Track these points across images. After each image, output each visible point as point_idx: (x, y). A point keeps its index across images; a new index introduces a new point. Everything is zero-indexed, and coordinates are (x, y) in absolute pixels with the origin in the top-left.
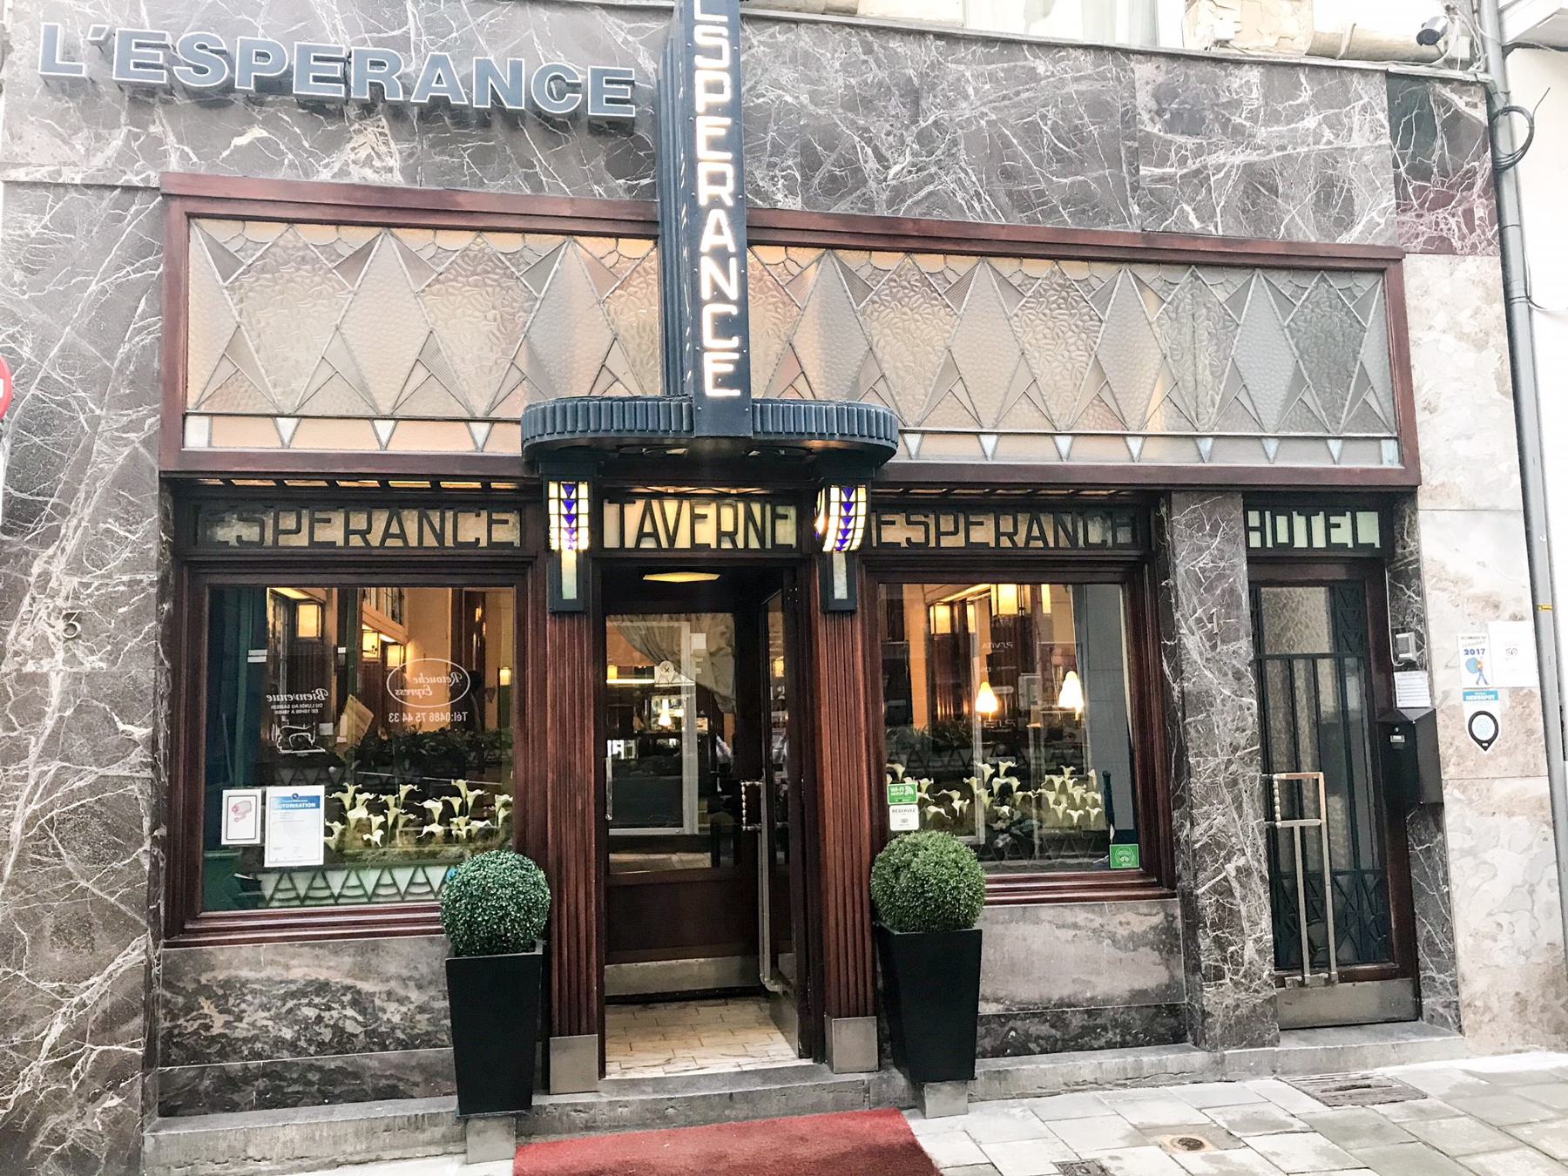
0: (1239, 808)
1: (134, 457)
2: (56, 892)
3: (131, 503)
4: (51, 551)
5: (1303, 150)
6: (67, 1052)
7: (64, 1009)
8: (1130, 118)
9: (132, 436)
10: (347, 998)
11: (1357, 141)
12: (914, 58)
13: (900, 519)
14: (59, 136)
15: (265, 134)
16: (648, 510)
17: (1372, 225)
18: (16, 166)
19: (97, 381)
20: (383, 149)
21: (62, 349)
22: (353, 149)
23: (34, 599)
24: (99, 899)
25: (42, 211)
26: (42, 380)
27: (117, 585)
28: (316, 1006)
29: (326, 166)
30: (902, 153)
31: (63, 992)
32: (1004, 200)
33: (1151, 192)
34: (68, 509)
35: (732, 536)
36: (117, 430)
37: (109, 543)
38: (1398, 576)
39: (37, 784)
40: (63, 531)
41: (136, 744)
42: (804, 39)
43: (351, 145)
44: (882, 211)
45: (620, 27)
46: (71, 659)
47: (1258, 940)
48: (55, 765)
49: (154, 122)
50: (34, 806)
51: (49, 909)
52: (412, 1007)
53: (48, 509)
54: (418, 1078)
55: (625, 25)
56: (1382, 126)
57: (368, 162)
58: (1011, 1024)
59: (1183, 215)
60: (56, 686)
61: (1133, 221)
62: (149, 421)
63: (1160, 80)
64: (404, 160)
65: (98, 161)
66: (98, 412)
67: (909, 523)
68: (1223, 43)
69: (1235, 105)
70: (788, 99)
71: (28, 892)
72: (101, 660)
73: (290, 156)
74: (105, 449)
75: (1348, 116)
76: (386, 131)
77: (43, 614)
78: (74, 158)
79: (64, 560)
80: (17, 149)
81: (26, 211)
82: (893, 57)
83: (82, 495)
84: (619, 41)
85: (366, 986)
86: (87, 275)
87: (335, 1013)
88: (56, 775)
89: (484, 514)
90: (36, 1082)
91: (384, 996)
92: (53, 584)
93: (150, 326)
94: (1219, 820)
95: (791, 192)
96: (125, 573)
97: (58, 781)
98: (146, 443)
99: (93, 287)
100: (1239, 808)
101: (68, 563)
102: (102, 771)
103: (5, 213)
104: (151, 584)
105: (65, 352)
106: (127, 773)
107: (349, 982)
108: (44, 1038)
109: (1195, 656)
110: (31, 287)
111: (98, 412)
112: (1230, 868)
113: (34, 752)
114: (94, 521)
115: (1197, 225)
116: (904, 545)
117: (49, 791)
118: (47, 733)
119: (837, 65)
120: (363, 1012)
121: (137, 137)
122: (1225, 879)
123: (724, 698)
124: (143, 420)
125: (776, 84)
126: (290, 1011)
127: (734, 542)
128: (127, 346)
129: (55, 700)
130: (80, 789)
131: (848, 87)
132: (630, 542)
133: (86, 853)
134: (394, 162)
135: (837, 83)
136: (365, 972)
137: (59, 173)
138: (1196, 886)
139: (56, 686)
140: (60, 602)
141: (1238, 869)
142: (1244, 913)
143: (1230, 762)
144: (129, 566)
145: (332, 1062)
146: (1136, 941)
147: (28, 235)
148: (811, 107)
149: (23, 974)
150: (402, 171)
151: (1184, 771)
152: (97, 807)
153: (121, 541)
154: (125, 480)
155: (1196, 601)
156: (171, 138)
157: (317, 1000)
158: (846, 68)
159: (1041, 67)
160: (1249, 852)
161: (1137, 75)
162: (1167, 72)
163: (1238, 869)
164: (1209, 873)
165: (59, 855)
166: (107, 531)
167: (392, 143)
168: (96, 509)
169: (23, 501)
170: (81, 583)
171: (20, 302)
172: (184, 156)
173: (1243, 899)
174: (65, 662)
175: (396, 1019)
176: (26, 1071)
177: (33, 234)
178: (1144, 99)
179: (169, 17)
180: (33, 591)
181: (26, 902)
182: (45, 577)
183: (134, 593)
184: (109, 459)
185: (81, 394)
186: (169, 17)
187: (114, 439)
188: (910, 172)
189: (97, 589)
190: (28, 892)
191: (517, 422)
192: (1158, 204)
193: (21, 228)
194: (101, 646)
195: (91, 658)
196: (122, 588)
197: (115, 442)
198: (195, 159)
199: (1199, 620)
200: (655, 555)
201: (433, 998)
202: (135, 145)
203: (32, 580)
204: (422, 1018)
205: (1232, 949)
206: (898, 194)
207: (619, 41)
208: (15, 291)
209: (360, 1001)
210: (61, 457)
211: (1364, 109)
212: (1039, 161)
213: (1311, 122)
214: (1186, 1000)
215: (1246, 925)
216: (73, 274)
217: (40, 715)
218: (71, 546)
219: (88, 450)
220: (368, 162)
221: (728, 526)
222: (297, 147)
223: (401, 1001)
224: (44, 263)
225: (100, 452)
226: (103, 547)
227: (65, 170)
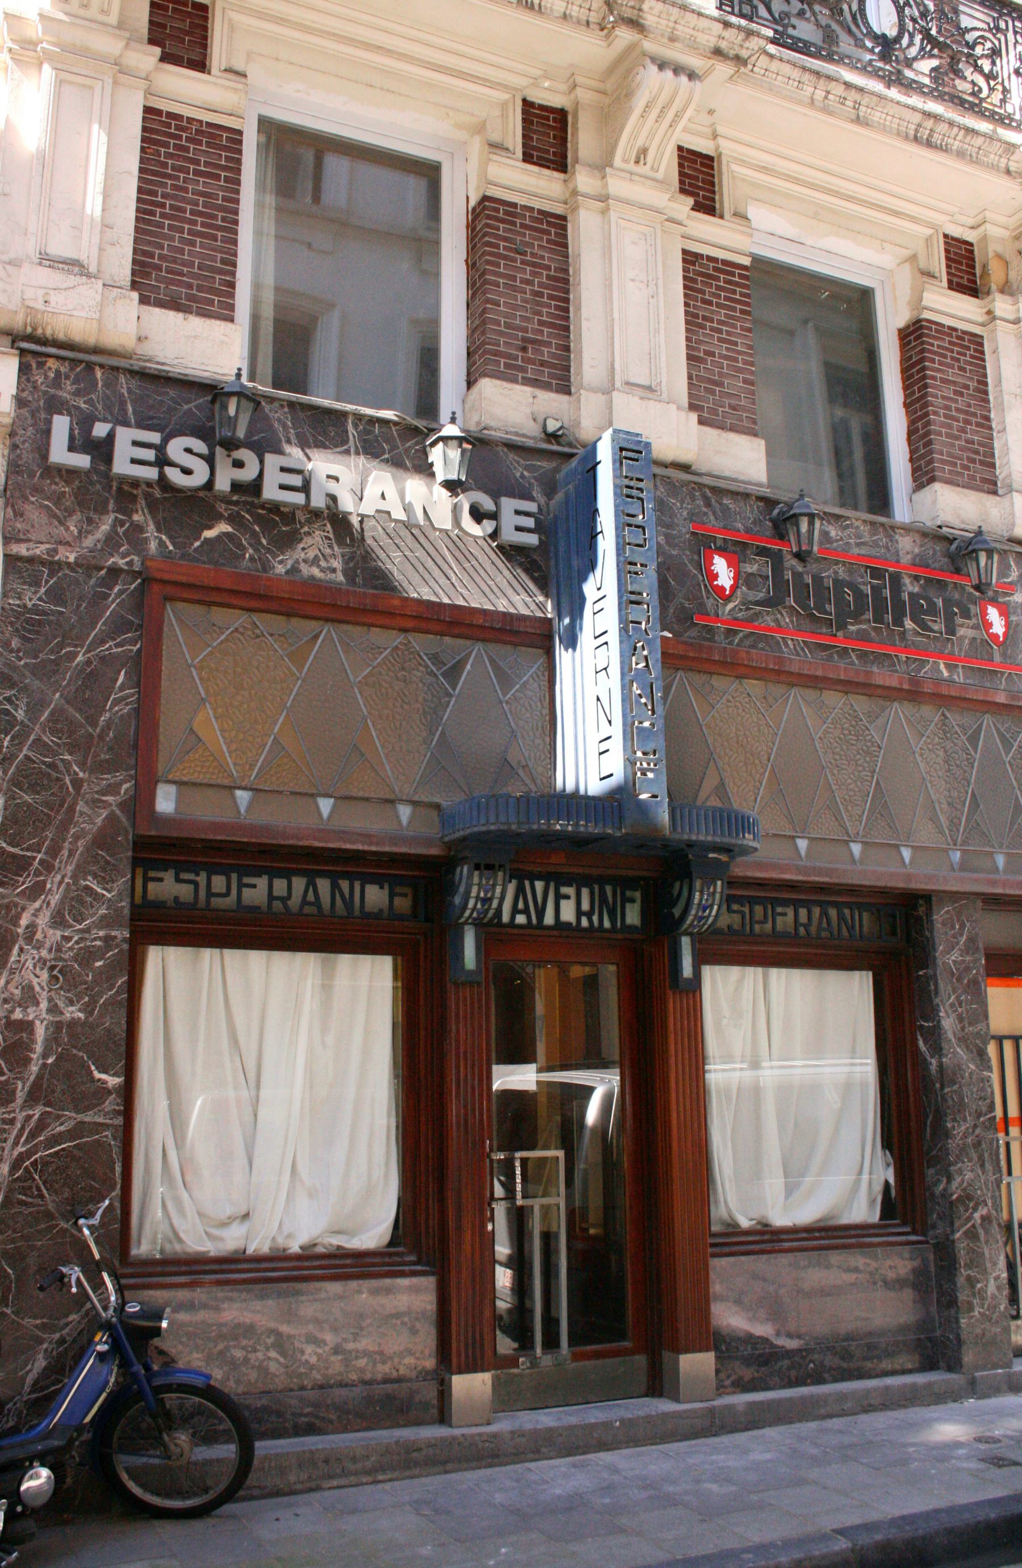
0: (982, 1165)
1: (111, 818)
2: (38, 1231)
3: (107, 862)
4: (37, 904)
6: (48, 1387)
7: (45, 1346)
9: (110, 799)
10: (270, 1341)
14: (55, 516)
15: (230, 529)
16: (520, 891)
18: (19, 541)
19: (80, 746)
20: (328, 551)
21: (52, 714)
22: (303, 549)
23: (21, 950)
25: (37, 584)
26: (34, 741)
27: (95, 939)
28: (243, 1348)
29: (281, 562)
31: (44, 1327)
34: (53, 866)
36: (97, 792)
37: (89, 899)
39: (23, 1128)
40: (48, 886)
41: (109, 1092)
43: (301, 546)
45: (518, 463)
46: (53, 1009)
47: (997, 1278)
48: (37, 1112)
49: (137, 511)
50: (21, 1149)
51: (32, 1248)
52: (327, 1348)
53: (36, 863)
54: (333, 1417)
55: (522, 462)
57: (315, 561)
58: (810, 1357)
60: (40, 1032)
62: (125, 786)
63: (917, 550)
64: (346, 562)
65: (89, 542)
66: (81, 775)
71: (14, 1231)
72: (80, 1010)
73: (251, 551)
74: (86, 809)
76: (331, 536)
77: (30, 964)
78: (69, 539)
79: (48, 914)
80: (19, 526)
81: (24, 583)
82: (726, 510)
83: (65, 853)
84: (518, 475)
86: (76, 646)
87: (260, 1355)
88: (40, 1120)
90: (19, 1417)
91: (303, 1339)
92: (39, 936)
93: (128, 697)
94: (969, 1176)
96: (101, 928)
97: (42, 1125)
98: (122, 805)
99: (80, 658)
100: (982, 1165)
101: (53, 917)
102: (80, 1117)
103: (4, 584)
104: (124, 940)
105: (57, 715)
106: (101, 1120)
107: (272, 1325)
108: (28, 1373)
109: (950, 1036)
110: (27, 654)
111: (81, 775)
112: (977, 1215)
113: (20, 1095)
114: (75, 877)
115: (946, 674)
117: (33, 1135)
118: (32, 1078)
119: (685, 513)
120: (283, 1353)
121: (122, 524)
122: (974, 1226)
124: (120, 784)
126: (221, 1353)
127: (590, 921)
128: (108, 715)
129: (39, 1047)
130: (60, 1133)
133: (66, 1195)
134: (337, 564)
136: (290, 1316)
137: (55, 551)
138: (953, 1232)
139: (40, 1032)
140: (44, 953)
141: (983, 1218)
142: (987, 1255)
143: (975, 1126)
144: (105, 922)
146: (899, 1284)
147: (25, 606)
149: (9, 1311)
150: (345, 572)
151: (941, 1133)
152: (75, 1152)
153: (97, 897)
154: (103, 840)
155: (950, 988)
156: (152, 527)
157: (244, 1342)
158: (692, 516)
160: (990, 1203)
161: (900, 546)
162: (921, 546)
163: (983, 1218)
164: (962, 1221)
165: (41, 1196)
166: (87, 887)
167: (336, 548)
168: (78, 866)
169: (14, 856)
170: (63, 937)
171: (15, 668)
172: (161, 544)
173: (987, 1242)
174: (49, 1011)
175: (313, 1360)
176: (10, 1405)
177: (29, 604)
179: (152, 418)
180: (21, 942)
181: (13, 1241)
182: (32, 928)
183: (108, 947)
184: (90, 819)
185: (68, 757)
186: (152, 418)
187: (95, 801)
189: (77, 943)
190: (14, 1231)
193: (20, 598)
194: (80, 998)
195: (71, 1009)
196: (98, 943)
197: (96, 803)
198: (171, 548)
199: (952, 1005)
201: (345, 1340)
202: (121, 531)
203: (20, 931)
205: (979, 1286)
207: (518, 475)
208: (12, 657)
209: (281, 1342)
210: (49, 816)
214: (938, 1333)
215: (988, 1265)
216: (61, 646)
217: (28, 1061)
218: (55, 899)
219: (72, 810)
220: (315, 561)
221: (585, 906)
222: (256, 545)
224: (38, 633)
225: (82, 813)
226: (82, 902)
227: (61, 549)
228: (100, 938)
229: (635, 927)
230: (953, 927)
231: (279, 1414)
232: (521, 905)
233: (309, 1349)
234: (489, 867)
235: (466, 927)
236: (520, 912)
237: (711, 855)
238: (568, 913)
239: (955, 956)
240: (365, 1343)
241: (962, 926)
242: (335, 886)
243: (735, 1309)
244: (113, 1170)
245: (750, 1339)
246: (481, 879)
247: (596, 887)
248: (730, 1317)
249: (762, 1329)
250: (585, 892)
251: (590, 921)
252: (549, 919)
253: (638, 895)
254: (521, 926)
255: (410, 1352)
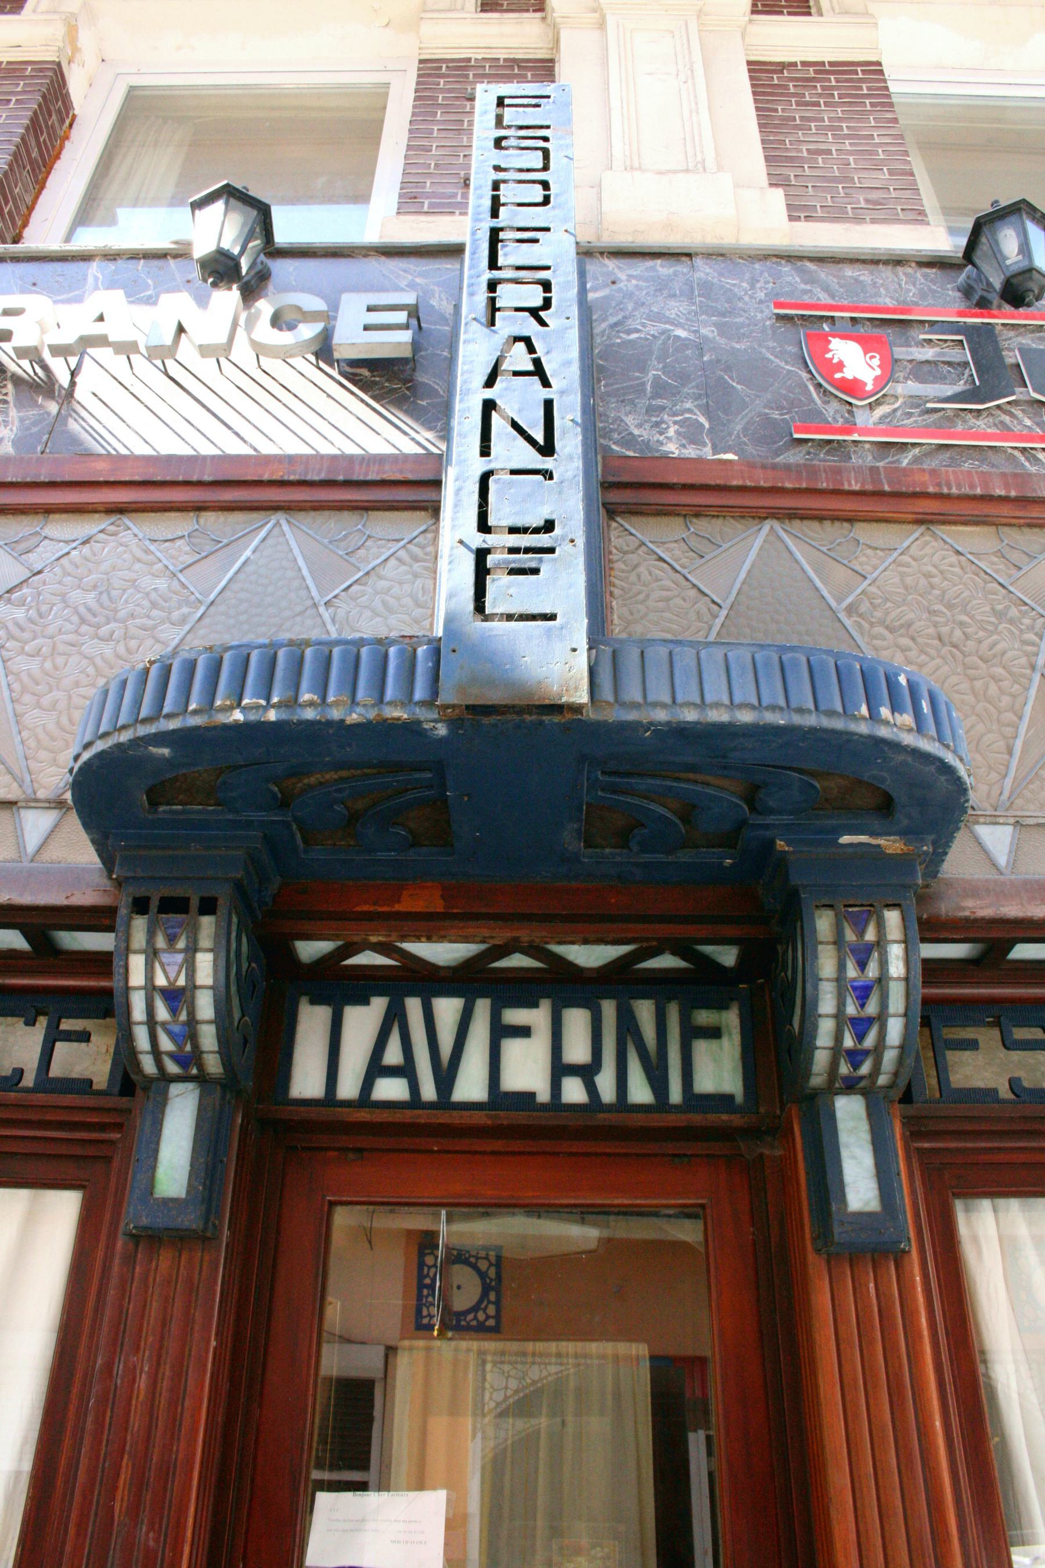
13: (988, 1037)
16: (395, 1017)
35: (587, 1073)
38: (848, 741)
67: (1009, 1044)
70: (682, 333)
89: (43, 1022)
116: (1005, 1093)
123: (61, 386)
125: (659, 318)
127: (591, 1089)
132: (348, 1088)
148: (723, 341)
188: (910, 415)
191: (129, 358)
200: (408, 1116)
221: (577, 1051)
229: (725, 1100)
232: (393, 1055)
234: (174, 905)
235: (175, 1089)
236: (393, 1072)
237: (845, 839)
238: (526, 1069)
246: (151, 935)
247: (609, 1009)
251: (591, 1089)
252: (471, 1086)
253: (731, 1019)
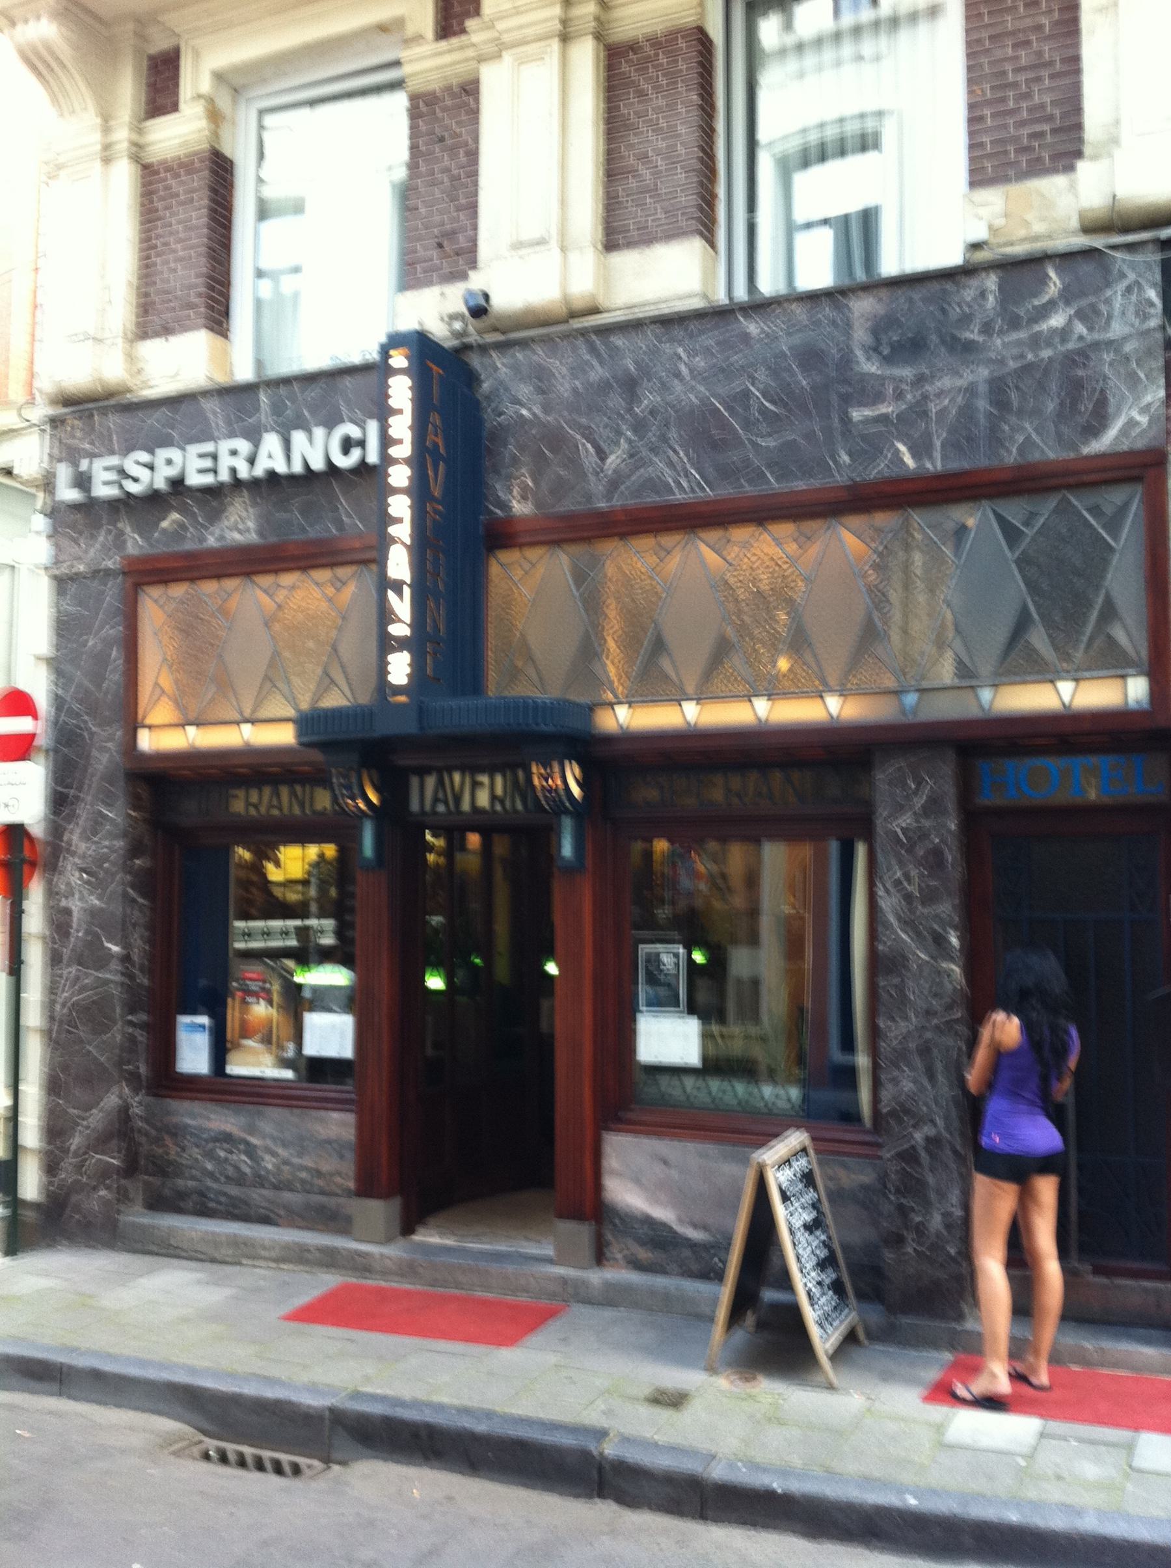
5: (1046, 353)
8: (847, 360)
9: (109, 745)
11: (1117, 329)
12: (630, 353)
16: (440, 783)
17: (1131, 423)
24: (96, 1058)
30: (617, 444)
32: (710, 471)
33: (864, 438)
42: (539, 355)
44: (602, 505)
54: (282, 1212)
56: (1152, 304)
59: (897, 458)
61: (844, 466)
68: (976, 246)
69: (966, 320)
70: (524, 412)
75: (1108, 302)
85: (254, 1140)
94: (907, 1086)
95: (524, 498)
97: (77, 979)
109: (892, 919)
120: (250, 1157)
131: (575, 390)
132: (428, 807)
135: (564, 387)
137: (72, 566)
141: (928, 1139)
145: (234, 1191)
154: (109, 779)
159: (753, 328)
163: (928, 1139)
175: (270, 1166)
178: (861, 335)
192: (870, 444)
196: (105, 850)
204: (286, 1168)
206: (614, 484)
209: (250, 1151)
211: (1129, 290)
212: (747, 424)
213: (1057, 320)
215: (933, 1196)
221: (499, 791)
223: (274, 1154)
228: (106, 847)
230: (904, 785)
231: (246, 1203)
233: (267, 1157)
238: (483, 799)
239: (906, 820)
240: (307, 1162)
241: (919, 783)
242: (293, 794)
243: (630, 1185)
244: (114, 1011)
245: (648, 1221)
248: (626, 1193)
249: (663, 1213)
250: (499, 780)
252: (466, 806)
254: (442, 814)
255: (339, 1174)
